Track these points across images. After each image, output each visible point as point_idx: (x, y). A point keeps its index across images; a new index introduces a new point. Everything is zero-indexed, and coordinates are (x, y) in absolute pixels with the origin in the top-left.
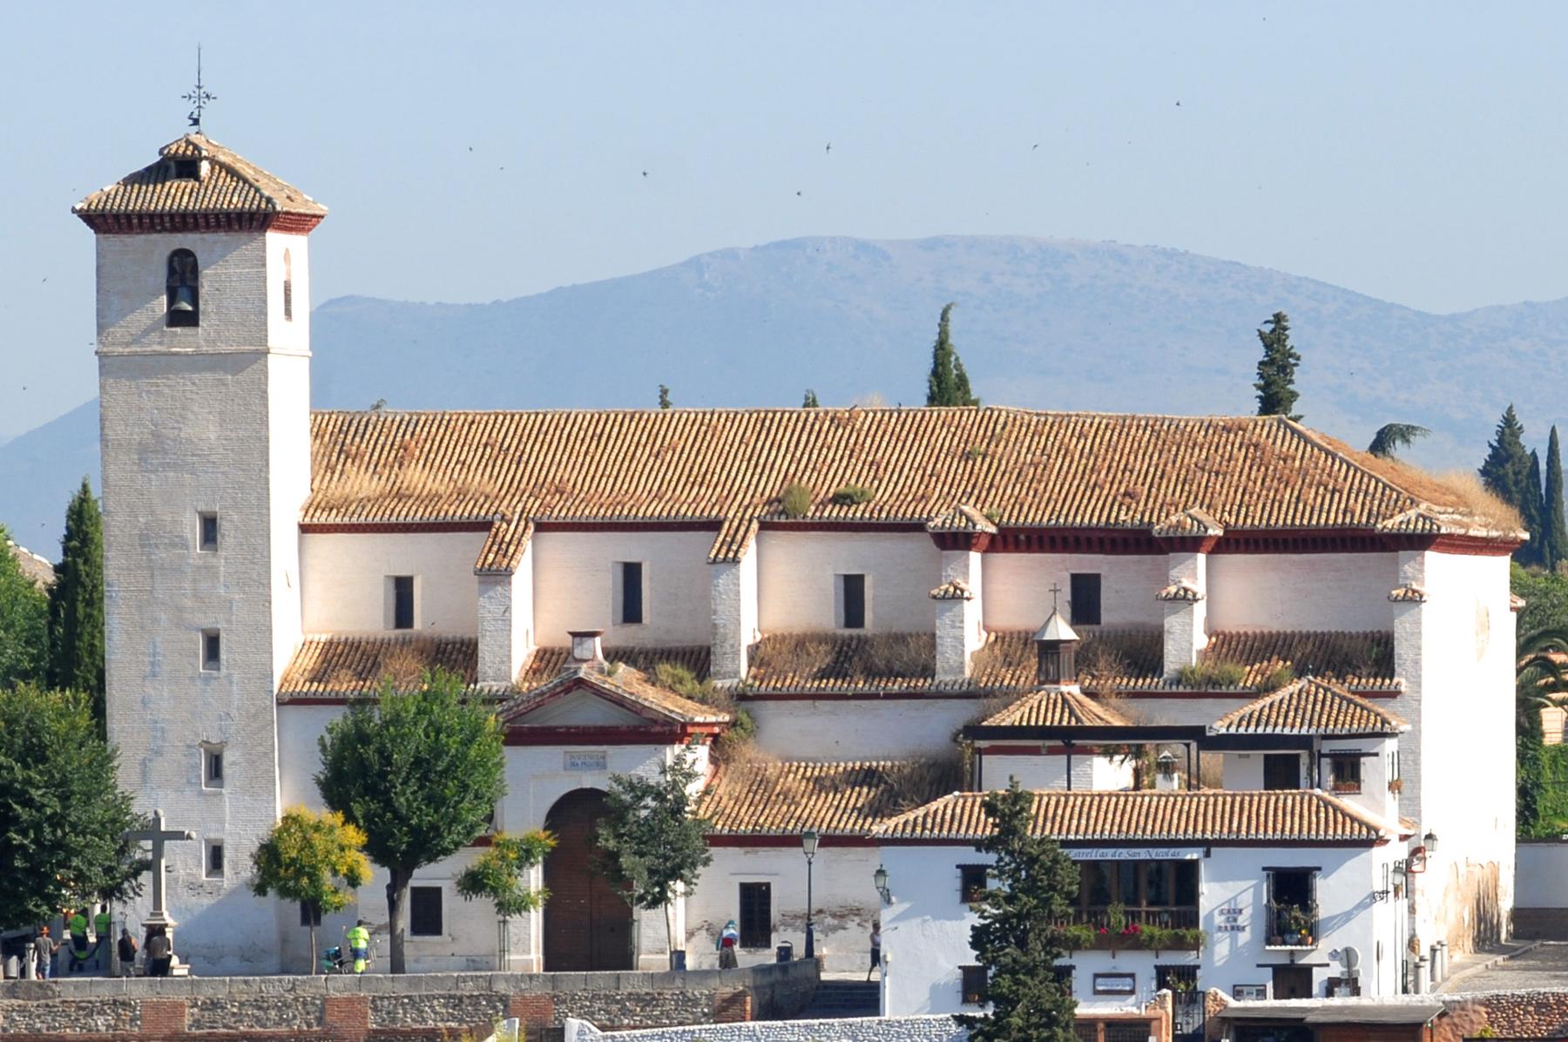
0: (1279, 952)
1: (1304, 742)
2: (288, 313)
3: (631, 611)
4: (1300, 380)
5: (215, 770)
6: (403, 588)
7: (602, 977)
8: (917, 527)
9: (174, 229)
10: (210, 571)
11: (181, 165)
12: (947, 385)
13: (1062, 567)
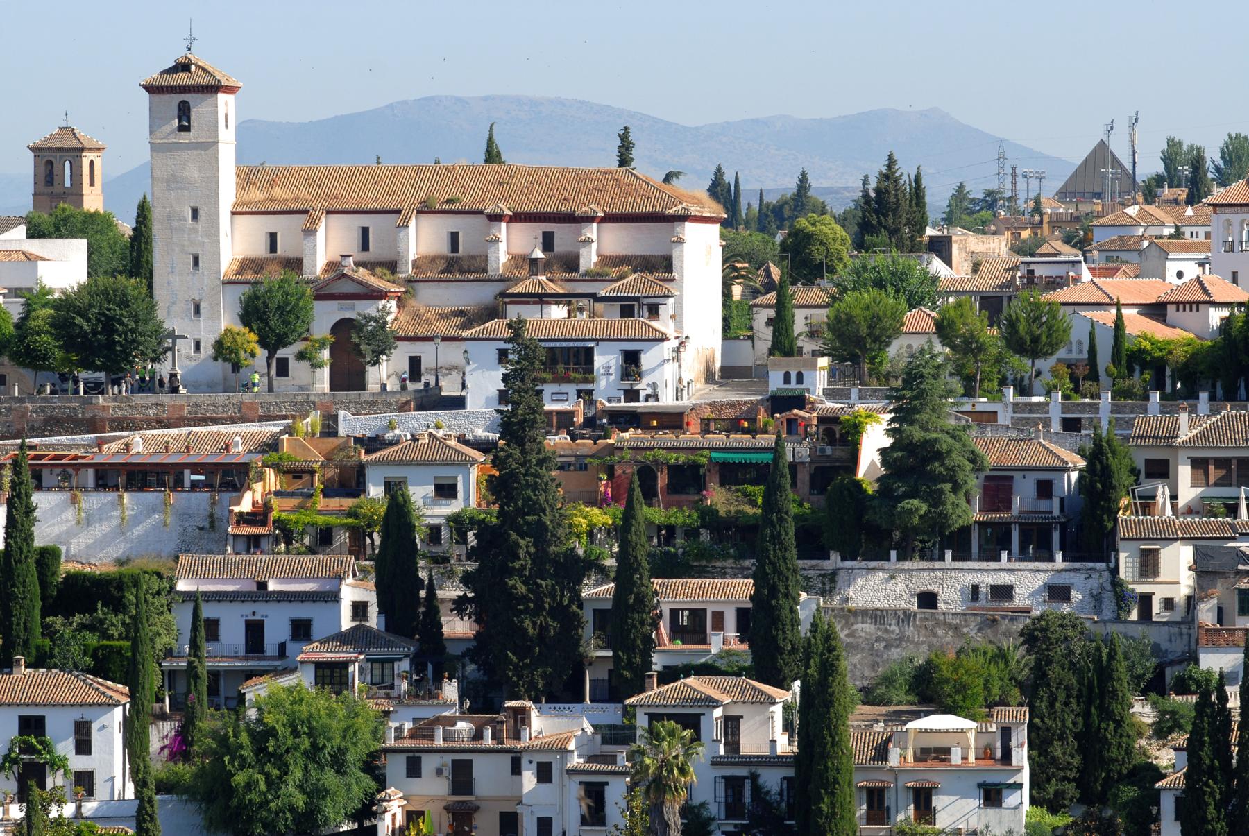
0: (626, 384)
1: (636, 299)
2: (92, 183)
3: (365, 246)
4: (635, 153)
5: (197, 311)
6: (273, 237)
7: (353, 394)
8: (481, 212)
9: (181, 92)
10: (195, 231)
11: (183, 67)
12: (492, 155)
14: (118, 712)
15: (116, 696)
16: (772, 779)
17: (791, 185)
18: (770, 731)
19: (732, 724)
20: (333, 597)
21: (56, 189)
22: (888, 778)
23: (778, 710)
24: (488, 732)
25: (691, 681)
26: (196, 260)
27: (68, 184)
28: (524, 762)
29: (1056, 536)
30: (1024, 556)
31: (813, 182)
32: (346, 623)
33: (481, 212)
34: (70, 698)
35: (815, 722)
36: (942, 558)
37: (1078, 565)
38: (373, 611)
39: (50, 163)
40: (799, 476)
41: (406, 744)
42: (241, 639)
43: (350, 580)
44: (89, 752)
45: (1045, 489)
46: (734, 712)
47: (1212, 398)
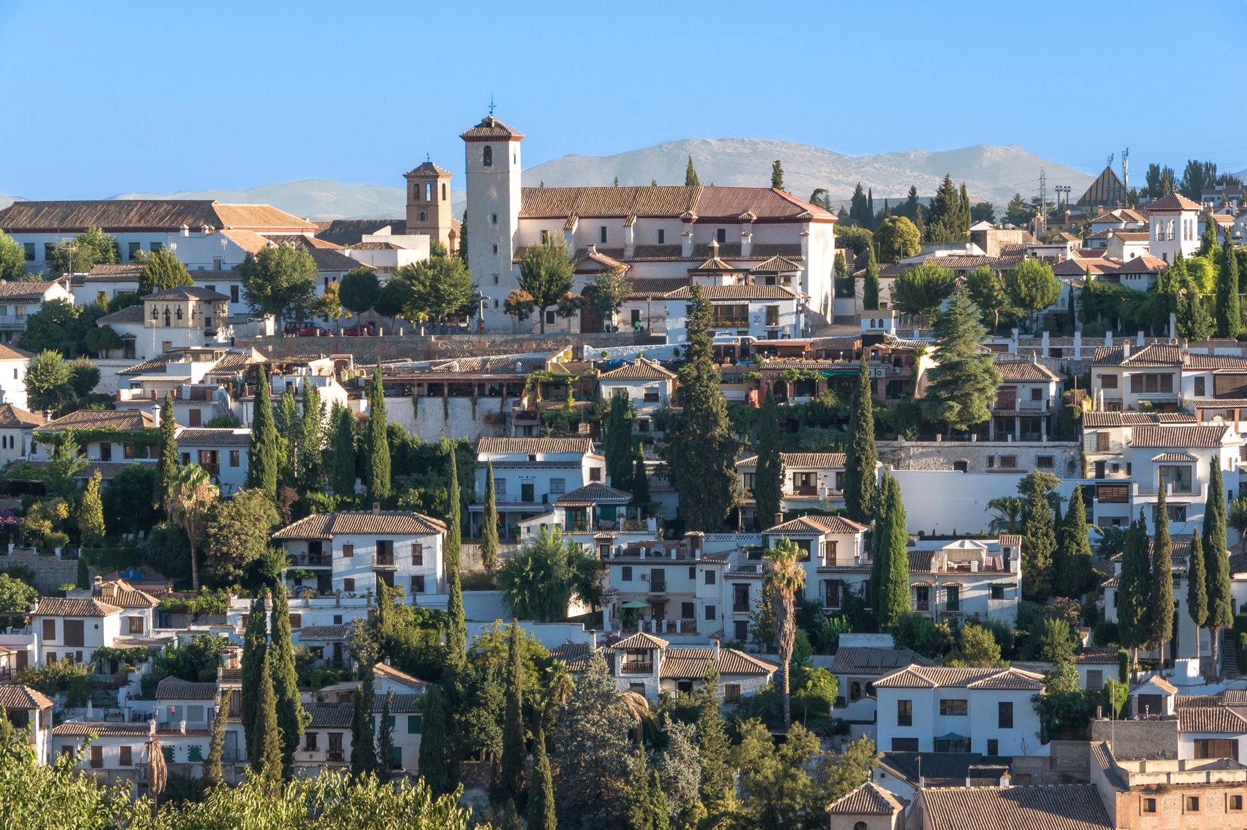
1: (776, 273)
2: (444, 198)
3: (604, 240)
4: (784, 178)
5: (496, 281)
6: (661, 233)
7: (594, 335)
11: (487, 123)
13: (715, 227)
14: (439, 538)
15: (438, 528)
16: (856, 582)
17: (905, 195)
18: (850, 547)
19: (831, 546)
20: (577, 465)
21: (421, 202)
22: (930, 581)
23: (859, 536)
24: (674, 552)
25: (805, 519)
26: (495, 248)
27: (429, 199)
28: (698, 571)
29: (1044, 425)
30: (1023, 439)
31: (919, 194)
32: (587, 481)
33: (677, 217)
34: (409, 529)
35: (879, 545)
36: (970, 440)
37: (1057, 443)
38: (603, 473)
39: (417, 185)
40: (879, 387)
41: (622, 559)
42: (519, 492)
43: (589, 453)
44: (421, 564)
45: (1037, 394)
46: (832, 538)
47: (1146, 336)
